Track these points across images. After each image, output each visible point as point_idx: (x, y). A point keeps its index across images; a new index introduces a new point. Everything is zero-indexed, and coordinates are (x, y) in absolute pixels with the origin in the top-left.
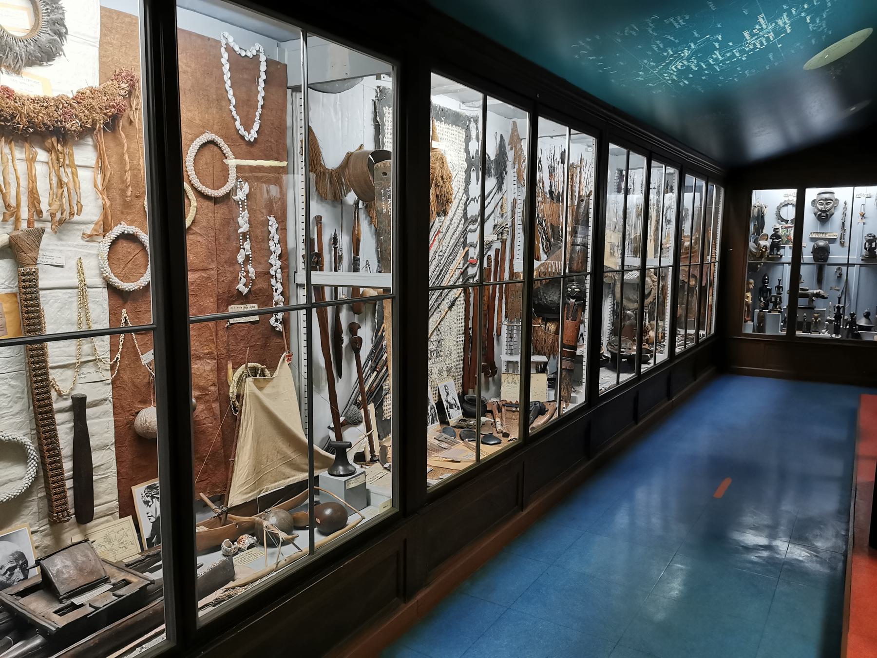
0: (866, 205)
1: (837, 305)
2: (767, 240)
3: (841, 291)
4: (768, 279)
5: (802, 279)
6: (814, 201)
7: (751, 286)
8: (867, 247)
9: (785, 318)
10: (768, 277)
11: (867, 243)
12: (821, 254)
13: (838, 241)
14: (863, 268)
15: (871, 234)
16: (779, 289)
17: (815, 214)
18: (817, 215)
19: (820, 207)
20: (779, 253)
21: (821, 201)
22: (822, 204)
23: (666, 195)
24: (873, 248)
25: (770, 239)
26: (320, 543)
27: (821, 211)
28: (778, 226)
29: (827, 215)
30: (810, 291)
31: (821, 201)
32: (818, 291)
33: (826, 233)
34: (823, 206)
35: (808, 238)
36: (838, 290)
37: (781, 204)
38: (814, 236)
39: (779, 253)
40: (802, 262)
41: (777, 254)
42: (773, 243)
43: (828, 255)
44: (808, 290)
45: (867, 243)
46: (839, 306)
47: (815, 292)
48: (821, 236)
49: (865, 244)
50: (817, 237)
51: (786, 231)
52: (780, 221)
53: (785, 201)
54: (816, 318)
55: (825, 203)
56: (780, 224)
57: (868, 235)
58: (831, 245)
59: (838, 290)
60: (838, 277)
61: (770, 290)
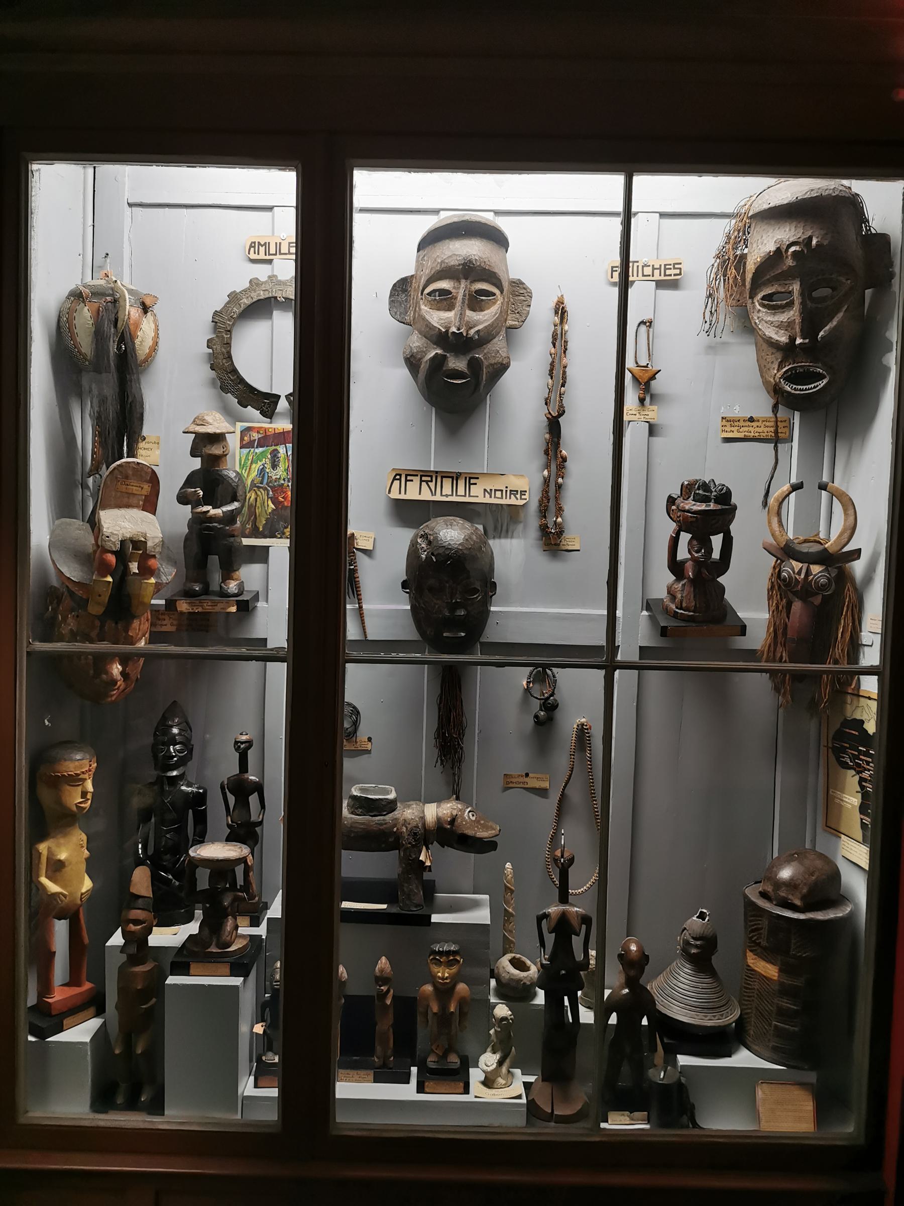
0: (656, 324)
1: (554, 910)
2: (150, 505)
3: (555, 797)
4: (187, 745)
5: (363, 732)
6: (402, 287)
7: (74, 798)
8: (683, 553)
9: (275, 993)
10: (186, 727)
11: (685, 537)
12: (762, 1042)
13: (533, 521)
14: (653, 676)
15: (705, 486)
16: (242, 802)
17: (412, 362)
18: (424, 367)
19: (438, 318)
20: (232, 586)
21: (444, 285)
22: (444, 300)
23: (766, 676)
24: (715, 563)
25: (183, 499)
26: (411, 530)
27: (442, 338)
28: (216, 423)
29: (475, 365)
30: (408, 813)
31: (444, 285)
32: (447, 809)
33: (471, 479)
34: (450, 315)
35: (381, 508)
36: (542, 793)
37: (234, 297)
38: (414, 492)
39: (232, 586)
40: (352, 632)
41: (224, 594)
42: (199, 523)
43: (486, 601)
44: (391, 806)
45: (685, 537)
46: (563, 918)
47: (432, 812)
48: (446, 493)
49: (674, 543)
50: (426, 495)
51: (267, 461)
52: (233, 400)
53: (254, 283)
54: (444, 991)
55: (460, 289)
56: (234, 418)
57: (687, 489)
58: (497, 545)
59: (542, 793)
60: (538, 721)
61: (200, 799)
